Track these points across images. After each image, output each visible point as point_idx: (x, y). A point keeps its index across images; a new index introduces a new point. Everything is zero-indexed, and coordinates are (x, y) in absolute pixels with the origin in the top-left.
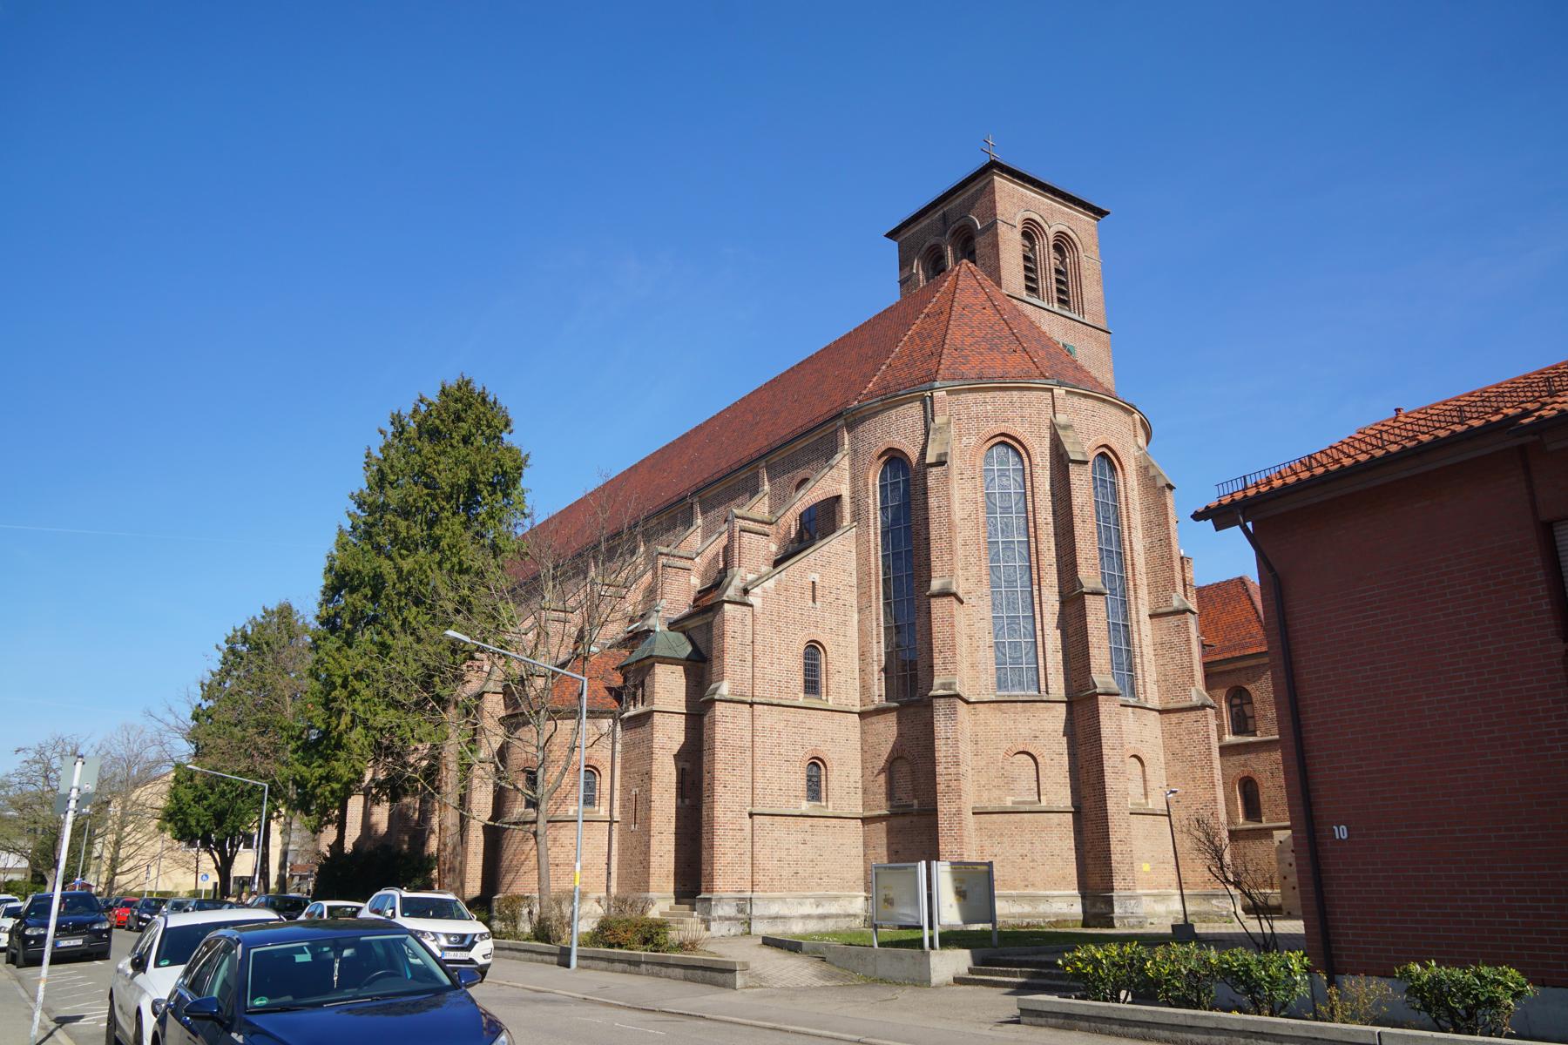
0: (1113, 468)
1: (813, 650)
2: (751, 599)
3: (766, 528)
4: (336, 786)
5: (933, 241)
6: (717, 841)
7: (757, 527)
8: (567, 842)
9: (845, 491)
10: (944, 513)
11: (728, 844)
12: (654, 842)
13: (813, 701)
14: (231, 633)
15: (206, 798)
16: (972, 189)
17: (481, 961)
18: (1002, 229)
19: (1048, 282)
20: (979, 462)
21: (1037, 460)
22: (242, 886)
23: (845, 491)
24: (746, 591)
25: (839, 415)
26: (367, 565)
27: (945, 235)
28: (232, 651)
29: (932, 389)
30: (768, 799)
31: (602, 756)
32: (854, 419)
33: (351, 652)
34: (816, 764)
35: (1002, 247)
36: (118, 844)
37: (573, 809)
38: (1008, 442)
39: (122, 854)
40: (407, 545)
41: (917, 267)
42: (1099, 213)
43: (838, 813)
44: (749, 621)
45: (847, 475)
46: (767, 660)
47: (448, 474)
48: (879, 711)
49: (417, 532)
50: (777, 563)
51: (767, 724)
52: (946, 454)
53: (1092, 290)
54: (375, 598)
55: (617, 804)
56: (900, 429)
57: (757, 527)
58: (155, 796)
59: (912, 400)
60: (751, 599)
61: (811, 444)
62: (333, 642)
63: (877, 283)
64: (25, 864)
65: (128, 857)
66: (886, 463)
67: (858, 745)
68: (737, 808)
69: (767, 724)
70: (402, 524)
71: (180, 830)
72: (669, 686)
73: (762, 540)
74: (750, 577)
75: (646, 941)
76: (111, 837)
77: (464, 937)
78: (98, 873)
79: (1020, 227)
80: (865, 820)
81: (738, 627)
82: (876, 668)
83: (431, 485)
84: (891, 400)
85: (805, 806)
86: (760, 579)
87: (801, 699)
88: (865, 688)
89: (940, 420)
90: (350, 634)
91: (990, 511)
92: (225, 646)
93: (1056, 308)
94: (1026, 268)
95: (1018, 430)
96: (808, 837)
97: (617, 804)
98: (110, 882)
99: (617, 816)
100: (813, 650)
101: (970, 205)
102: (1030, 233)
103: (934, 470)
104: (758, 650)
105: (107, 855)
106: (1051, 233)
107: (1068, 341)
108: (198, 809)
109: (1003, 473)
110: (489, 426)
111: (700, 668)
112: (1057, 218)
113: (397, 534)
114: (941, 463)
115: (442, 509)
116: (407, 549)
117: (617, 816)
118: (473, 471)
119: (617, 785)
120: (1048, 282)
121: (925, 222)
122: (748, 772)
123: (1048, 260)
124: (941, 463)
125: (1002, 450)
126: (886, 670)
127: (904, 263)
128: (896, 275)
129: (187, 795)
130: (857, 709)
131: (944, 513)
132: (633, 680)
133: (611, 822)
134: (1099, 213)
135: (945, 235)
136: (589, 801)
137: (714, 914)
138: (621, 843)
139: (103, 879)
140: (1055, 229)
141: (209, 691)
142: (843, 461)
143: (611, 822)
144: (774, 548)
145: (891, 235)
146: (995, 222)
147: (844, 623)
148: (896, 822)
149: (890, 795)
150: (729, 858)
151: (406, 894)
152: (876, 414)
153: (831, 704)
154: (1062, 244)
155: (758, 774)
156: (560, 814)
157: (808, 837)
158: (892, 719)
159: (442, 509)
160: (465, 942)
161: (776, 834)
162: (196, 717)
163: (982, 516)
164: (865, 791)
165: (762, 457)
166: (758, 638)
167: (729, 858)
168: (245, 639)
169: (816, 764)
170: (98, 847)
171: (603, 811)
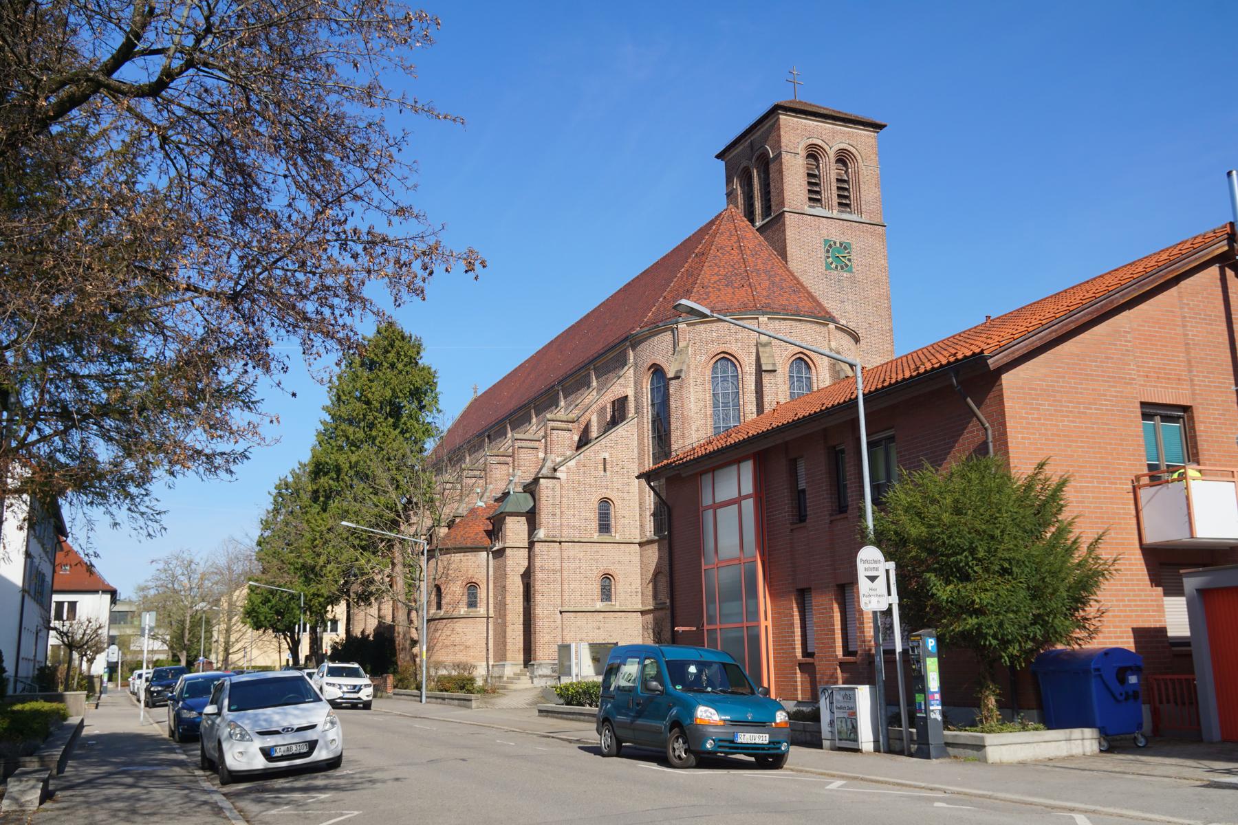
0: (809, 367)
1: (605, 503)
2: (558, 474)
3: (570, 426)
4: (321, 599)
5: (744, 163)
6: (538, 629)
7: (564, 425)
8: (460, 631)
9: (630, 392)
10: (679, 412)
11: (546, 630)
12: (509, 630)
13: (605, 538)
14: (278, 482)
15: (269, 601)
16: (767, 125)
17: (365, 698)
18: (786, 157)
19: (830, 192)
20: (708, 372)
21: (746, 369)
22: (132, 670)
23: (630, 392)
24: (555, 470)
25: (626, 339)
26: (330, 459)
27: (750, 161)
28: (280, 494)
29: (677, 323)
30: (573, 602)
31: (480, 577)
32: (635, 342)
33: (324, 515)
34: (607, 578)
35: (785, 173)
36: (228, 631)
37: (463, 610)
38: (726, 360)
39: (233, 639)
40: (355, 445)
41: (736, 184)
42: (877, 127)
43: (623, 608)
44: (557, 488)
45: (632, 381)
46: (571, 512)
47: (378, 393)
48: (650, 542)
49: (361, 435)
50: (578, 448)
51: (571, 554)
52: (681, 371)
53: (868, 191)
54: (337, 480)
55: (491, 606)
56: (658, 349)
57: (564, 425)
58: (241, 596)
59: (665, 330)
60: (558, 474)
61: (609, 360)
62: (316, 508)
63: (707, 193)
64: (166, 647)
65: (237, 641)
66: (653, 373)
67: (639, 564)
68: (551, 608)
69: (571, 554)
70: (351, 430)
71: (255, 624)
72: (516, 530)
73: (567, 434)
74: (558, 460)
75: (462, 688)
76: (223, 626)
77: (355, 686)
78: (217, 654)
79: (803, 153)
80: (643, 613)
81: (550, 493)
82: (648, 514)
83: (368, 403)
84: (655, 330)
85: (599, 605)
86: (566, 460)
87: (596, 536)
88: (642, 527)
89: (682, 344)
90: (325, 503)
91: (716, 406)
92: (274, 492)
93: (835, 214)
94: (809, 183)
95: (734, 348)
96: (601, 625)
97: (491, 606)
98: (226, 660)
99: (491, 613)
100: (605, 503)
101: (765, 139)
102: (814, 154)
103: (673, 382)
104: (567, 506)
105: (222, 640)
106: (832, 153)
107: (844, 239)
108: (265, 609)
109: (724, 379)
110: (406, 355)
111: (532, 517)
112: (834, 137)
113: (348, 438)
114: (677, 377)
115: (375, 418)
116: (355, 446)
117: (491, 613)
118: (393, 390)
119: (491, 594)
120: (830, 192)
121: (739, 148)
122: (558, 586)
123: (830, 171)
124: (677, 377)
125: (723, 362)
126: (654, 515)
127: (729, 181)
128: (724, 190)
129: (258, 600)
130: (638, 541)
131: (679, 412)
132: (495, 529)
133: (488, 618)
134: (877, 127)
135: (750, 161)
136: (472, 604)
137: (536, 673)
138: (495, 630)
139: (221, 658)
140: (835, 148)
141: (266, 525)
142: (629, 372)
143: (488, 618)
144: (576, 438)
145: (720, 156)
146: (780, 153)
147: (628, 484)
148: (659, 613)
149: (655, 597)
150: (546, 640)
151: (331, 665)
152: (647, 339)
153: (618, 538)
154: (843, 158)
155: (566, 586)
156: (455, 614)
157: (601, 625)
158: (655, 546)
159: (375, 418)
160: (356, 689)
161: (579, 623)
162: (259, 544)
163: (710, 410)
164: (642, 594)
165: (590, 362)
166: (565, 500)
167: (546, 640)
168: (287, 486)
169: (607, 578)
170: (215, 634)
171: (481, 610)
